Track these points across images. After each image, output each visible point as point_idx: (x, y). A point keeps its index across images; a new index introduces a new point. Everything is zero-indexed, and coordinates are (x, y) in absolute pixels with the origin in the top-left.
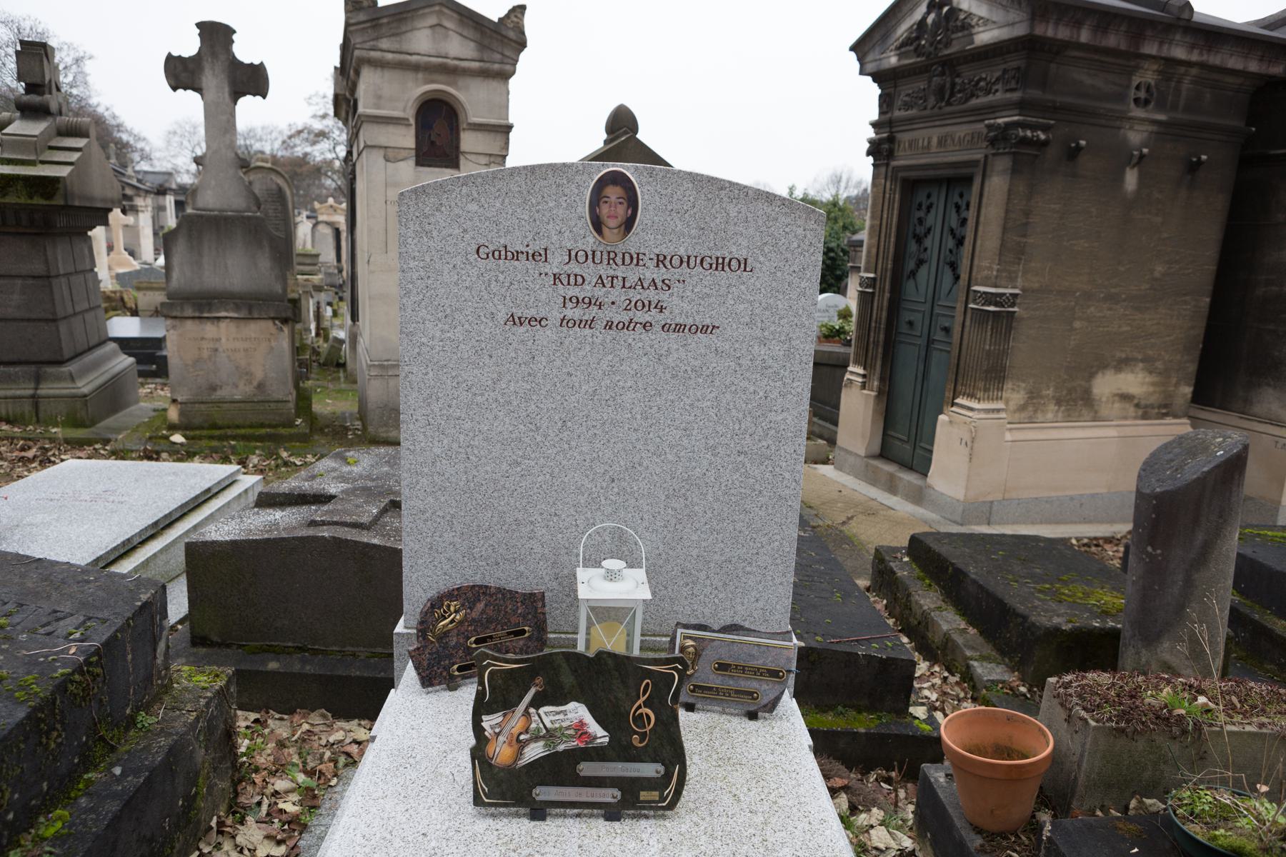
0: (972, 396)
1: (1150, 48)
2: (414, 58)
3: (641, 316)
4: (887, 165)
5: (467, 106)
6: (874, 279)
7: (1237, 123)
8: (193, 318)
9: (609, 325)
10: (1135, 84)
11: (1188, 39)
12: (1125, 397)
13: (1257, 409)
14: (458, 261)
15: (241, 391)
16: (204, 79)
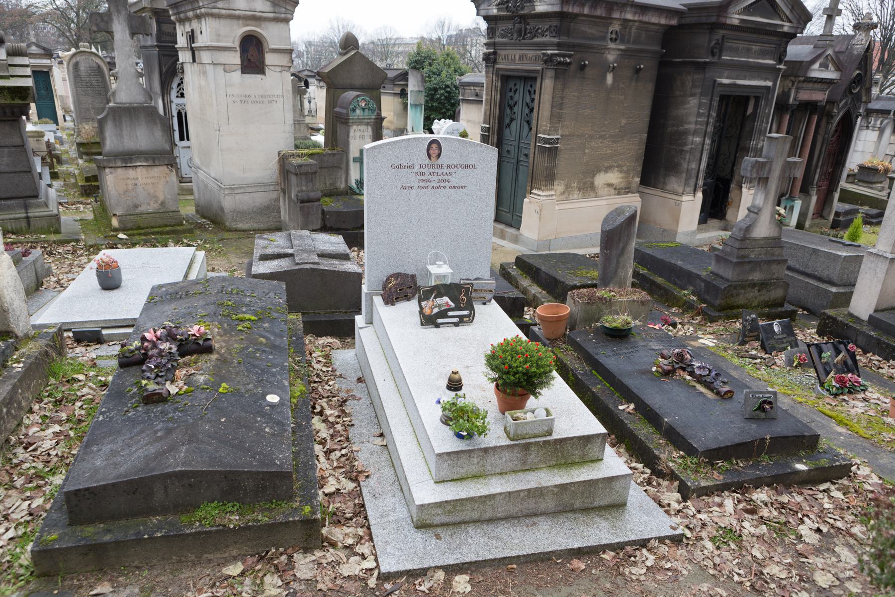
0: (540, 189)
1: (616, 15)
2: (237, 12)
3: (443, 184)
4: (493, 67)
5: (268, 39)
6: (489, 128)
7: (657, 48)
8: (122, 167)
9: (433, 188)
10: (610, 31)
11: (633, 10)
12: (609, 185)
13: (668, 187)
14: (385, 169)
15: (152, 207)
16: (114, 26)
